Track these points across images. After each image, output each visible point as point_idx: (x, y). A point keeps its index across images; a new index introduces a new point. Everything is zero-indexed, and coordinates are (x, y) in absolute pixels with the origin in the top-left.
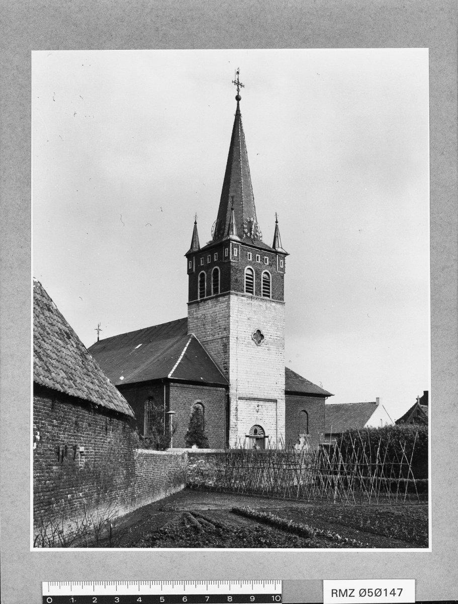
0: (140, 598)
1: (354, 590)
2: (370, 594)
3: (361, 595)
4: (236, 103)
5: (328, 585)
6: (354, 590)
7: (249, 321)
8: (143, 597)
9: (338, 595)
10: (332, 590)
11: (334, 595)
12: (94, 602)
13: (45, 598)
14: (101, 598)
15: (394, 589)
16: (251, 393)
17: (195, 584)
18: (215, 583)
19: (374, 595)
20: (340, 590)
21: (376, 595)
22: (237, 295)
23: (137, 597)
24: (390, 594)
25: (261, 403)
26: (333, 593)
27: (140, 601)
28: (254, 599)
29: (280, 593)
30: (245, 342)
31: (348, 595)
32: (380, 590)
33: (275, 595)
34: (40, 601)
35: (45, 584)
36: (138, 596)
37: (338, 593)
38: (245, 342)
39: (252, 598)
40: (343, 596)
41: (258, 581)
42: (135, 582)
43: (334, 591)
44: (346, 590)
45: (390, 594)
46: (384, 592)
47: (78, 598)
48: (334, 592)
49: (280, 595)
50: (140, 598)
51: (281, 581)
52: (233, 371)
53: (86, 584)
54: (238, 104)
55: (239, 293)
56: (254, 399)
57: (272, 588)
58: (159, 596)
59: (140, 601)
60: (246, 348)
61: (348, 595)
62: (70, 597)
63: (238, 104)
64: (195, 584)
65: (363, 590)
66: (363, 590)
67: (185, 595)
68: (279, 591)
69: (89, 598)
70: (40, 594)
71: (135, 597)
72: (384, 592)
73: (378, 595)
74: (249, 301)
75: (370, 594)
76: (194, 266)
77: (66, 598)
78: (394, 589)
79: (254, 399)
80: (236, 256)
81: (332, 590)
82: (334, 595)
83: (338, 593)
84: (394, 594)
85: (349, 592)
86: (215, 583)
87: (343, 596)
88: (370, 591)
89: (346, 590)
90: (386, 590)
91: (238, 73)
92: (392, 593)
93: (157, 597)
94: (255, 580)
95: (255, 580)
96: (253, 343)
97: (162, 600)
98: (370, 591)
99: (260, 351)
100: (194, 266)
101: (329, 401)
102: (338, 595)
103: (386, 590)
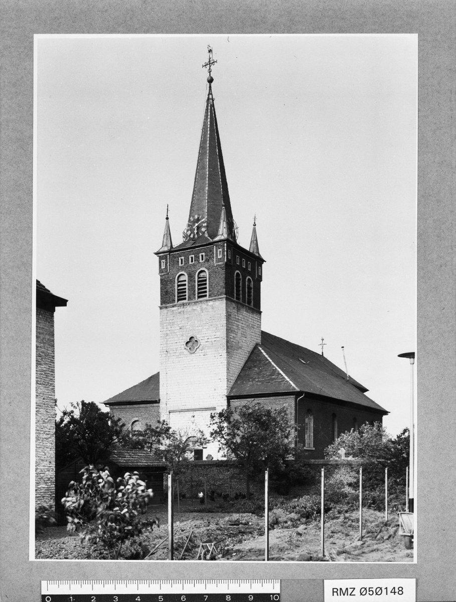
0: (139, 597)
1: (354, 589)
2: (371, 593)
3: (361, 594)
4: (208, 86)
5: (329, 585)
6: (354, 589)
7: (181, 330)
8: (141, 596)
9: (339, 594)
10: (333, 589)
11: (335, 594)
12: (92, 601)
13: (44, 596)
14: (99, 597)
15: (394, 588)
16: (184, 404)
17: (91, 583)
18: (202, 582)
19: (375, 593)
20: (341, 589)
21: (377, 594)
22: (166, 307)
23: (136, 596)
24: (391, 592)
25: (196, 413)
26: (333, 592)
27: (139, 600)
28: (252, 598)
29: (278, 592)
30: (177, 354)
31: (349, 594)
32: (381, 589)
33: (273, 594)
34: (40, 600)
35: (44, 583)
36: (137, 595)
37: (339, 592)
38: (177, 354)
39: (251, 597)
40: (344, 595)
41: (257, 581)
42: (134, 581)
43: (335, 590)
44: (347, 589)
45: (391, 592)
46: (384, 591)
47: (77, 597)
48: (335, 591)
49: (278, 594)
50: (139, 597)
51: (279, 580)
52: (163, 386)
53: (73, 583)
54: (210, 87)
55: (168, 305)
56: (188, 410)
57: (270, 588)
58: (225, 595)
59: (139, 600)
60: (177, 359)
61: (349, 594)
62: (69, 596)
63: (210, 87)
64: (91, 583)
65: (364, 589)
66: (364, 589)
67: (184, 595)
68: (277, 590)
69: (87, 598)
70: (39, 594)
71: (134, 596)
72: (384, 591)
73: (378, 594)
74: (181, 309)
75: (371, 593)
76: (215, 252)
77: (200, 596)
78: (394, 588)
79: (188, 410)
80: (164, 267)
81: (333, 589)
82: (335, 594)
83: (339, 592)
84: (395, 592)
85: (350, 591)
86: (202, 582)
87: (344, 595)
88: (371, 589)
89: (347, 589)
90: (387, 588)
91: (210, 51)
92: (393, 591)
93: (156, 596)
94: (156, 580)
95: (156, 580)
96: (186, 352)
97: (161, 599)
98: (371, 589)
99: (196, 359)
100: (215, 252)
101: (366, 394)
102: (339, 594)
103: (387, 588)
